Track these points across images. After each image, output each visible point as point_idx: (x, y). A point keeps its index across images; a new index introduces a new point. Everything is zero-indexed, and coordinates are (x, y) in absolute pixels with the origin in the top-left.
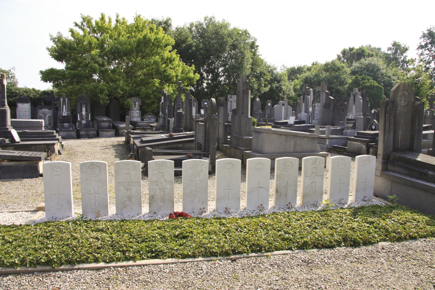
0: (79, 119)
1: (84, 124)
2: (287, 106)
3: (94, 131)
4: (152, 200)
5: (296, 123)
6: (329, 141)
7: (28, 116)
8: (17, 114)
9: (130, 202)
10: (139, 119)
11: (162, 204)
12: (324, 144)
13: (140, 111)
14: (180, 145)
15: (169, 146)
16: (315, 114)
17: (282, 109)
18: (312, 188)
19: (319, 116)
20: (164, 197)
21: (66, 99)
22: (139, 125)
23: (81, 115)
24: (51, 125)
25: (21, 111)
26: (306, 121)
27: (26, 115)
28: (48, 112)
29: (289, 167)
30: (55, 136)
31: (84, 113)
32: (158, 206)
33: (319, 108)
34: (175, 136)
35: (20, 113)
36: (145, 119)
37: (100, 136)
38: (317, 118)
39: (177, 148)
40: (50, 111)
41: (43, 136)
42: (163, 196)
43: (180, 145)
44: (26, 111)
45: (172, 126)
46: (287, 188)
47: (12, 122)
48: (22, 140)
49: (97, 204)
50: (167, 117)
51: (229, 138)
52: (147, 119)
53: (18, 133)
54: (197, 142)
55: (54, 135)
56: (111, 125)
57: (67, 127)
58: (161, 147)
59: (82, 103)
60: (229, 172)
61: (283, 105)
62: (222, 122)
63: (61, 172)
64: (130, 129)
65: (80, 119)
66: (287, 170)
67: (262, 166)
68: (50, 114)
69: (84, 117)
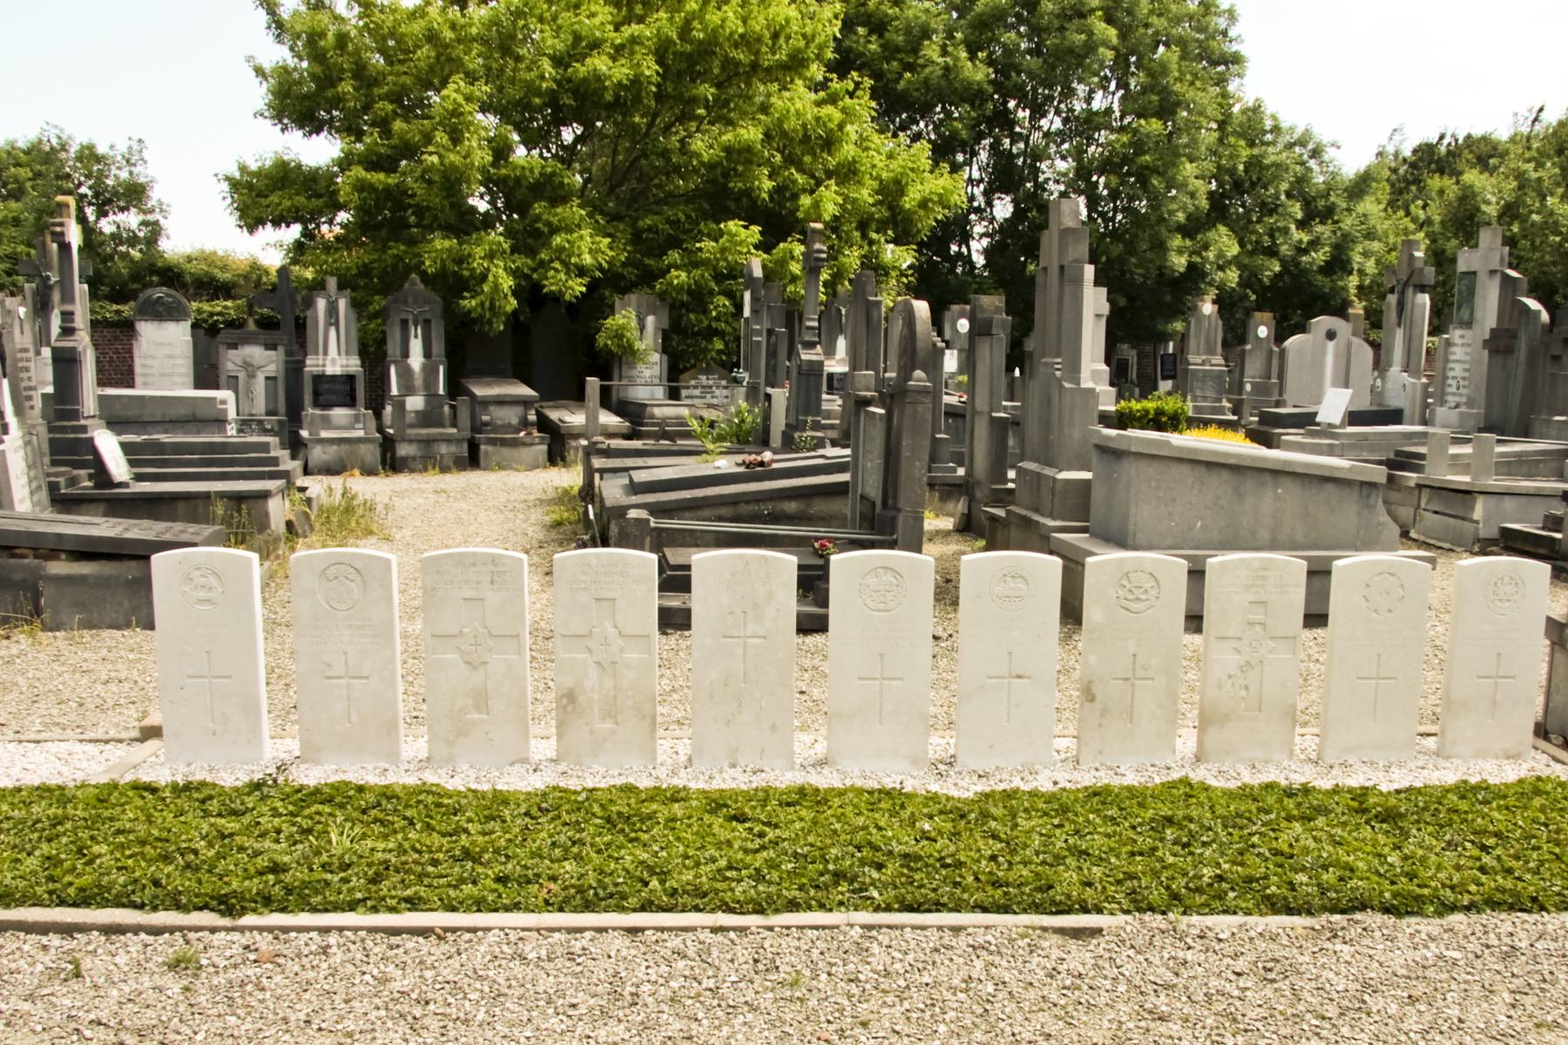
0: (395, 391)
1: (417, 412)
2: (1349, 345)
3: (459, 441)
4: (569, 709)
5: (1354, 418)
6: (1485, 508)
7: (181, 375)
8: (138, 369)
9: (480, 712)
10: (660, 392)
11: (609, 725)
12: (1463, 519)
13: (665, 357)
14: (791, 507)
15: (744, 509)
16: (1450, 381)
17: (1323, 354)
18: (1247, 688)
19: (1463, 391)
20: (615, 697)
21: (342, 304)
22: (653, 417)
23: (405, 373)
24: (275, 414)
25: (153, 357)
26: (1407, 413)
27: (171, 375)
28: (264, 360)
29: (1143, 597)
30: (275, 461)
31: (416, 360)
32: (592, 732)
33: (1468, 350)
34: (775, 466)
35: (149, 362)
36: (684, 393)
37: (482, 463)
38: (1457, 399)
39: (775, 519)
40: (272, 353)
41: (219, 458)
42: (611, 694)
43: (791, 507)
44: (171, 357)
45: (779, 422)
46: (1133, 685)
47: (102, 400)
48: (139, 478)
49: (354, 718)
50: (762, 381)
51: (1012, 481)
52: (697, 392)
53: (124, 446)
54: (860, 491)
55: (273, 454)
56: (532, 417)
57: (344, 422)
58: (706, 512)
59: (411, 317)
60: (882, 606)
61: (1331, 335)
62: (986, 408)
63: (220, 590)
64: (601, 435)
65: (399, 389)
66: (1135, 606)
67: (1023, 586)
68: (272, 369)
69: (418, 381)
